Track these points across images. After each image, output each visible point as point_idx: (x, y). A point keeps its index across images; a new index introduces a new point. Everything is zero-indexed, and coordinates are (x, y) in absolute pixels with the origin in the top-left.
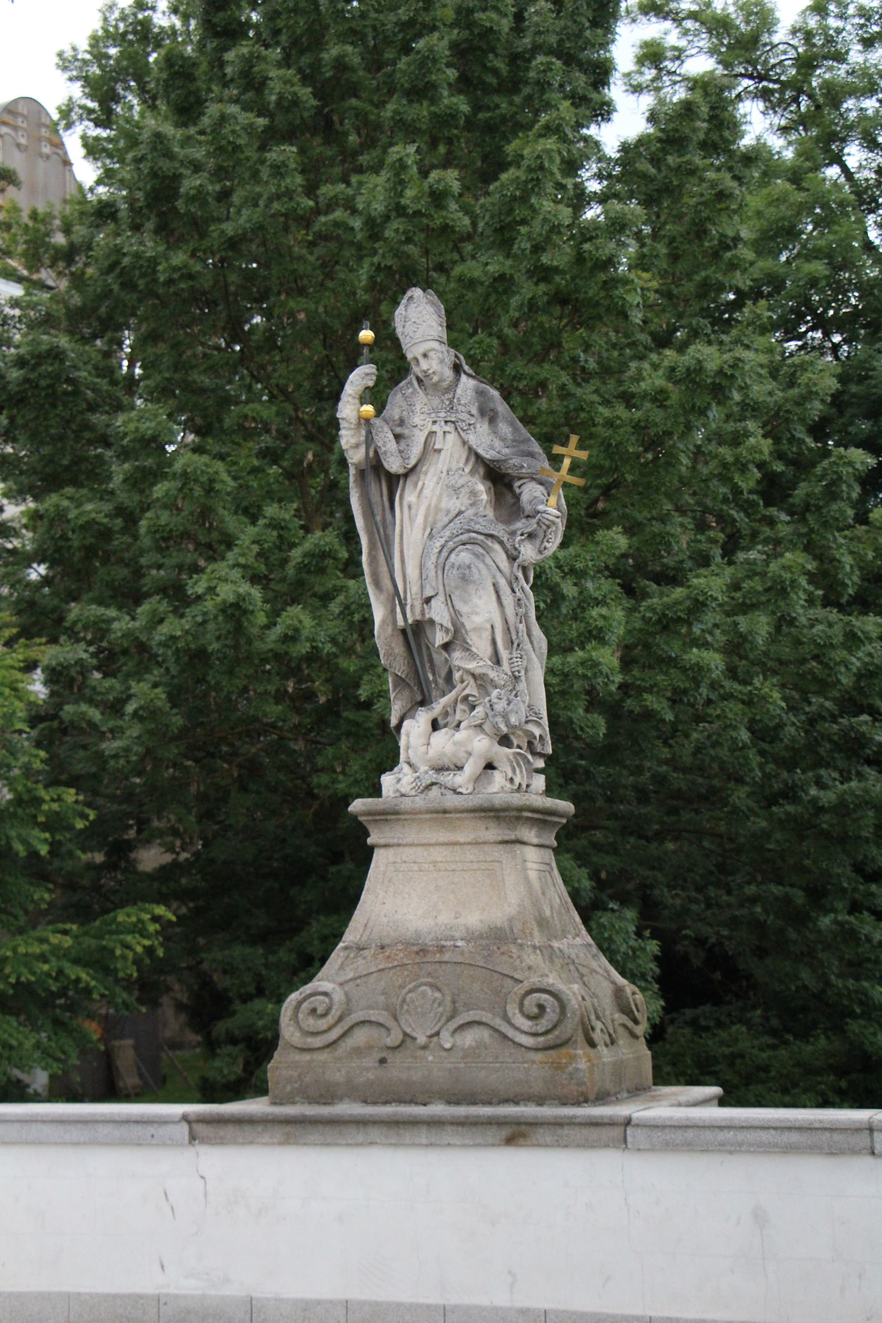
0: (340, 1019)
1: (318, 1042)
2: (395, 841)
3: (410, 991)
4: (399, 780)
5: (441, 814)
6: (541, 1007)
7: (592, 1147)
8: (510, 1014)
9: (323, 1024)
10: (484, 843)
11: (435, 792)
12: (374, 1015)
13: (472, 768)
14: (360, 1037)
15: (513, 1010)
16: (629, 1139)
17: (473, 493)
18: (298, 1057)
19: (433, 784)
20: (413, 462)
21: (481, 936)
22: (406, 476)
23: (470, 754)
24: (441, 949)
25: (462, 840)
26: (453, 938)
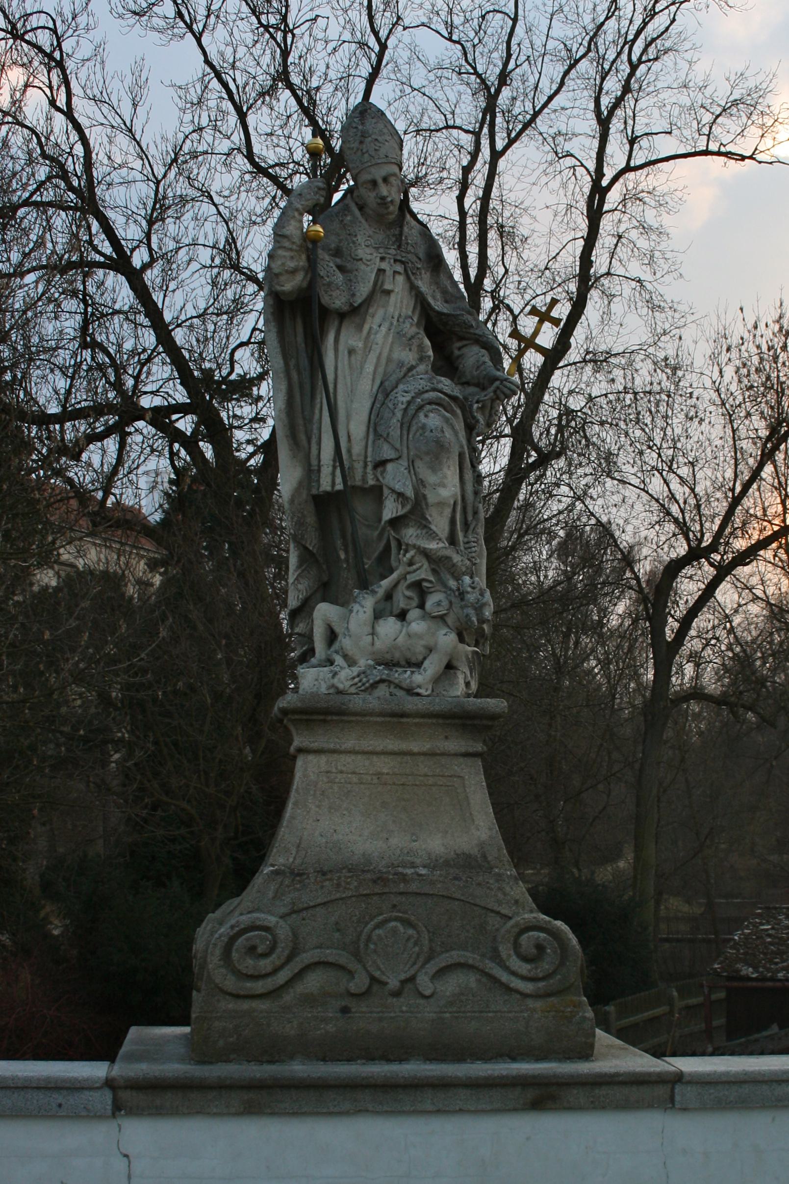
0: (289, 959)
1: (259, 987)
2: (332, 746)
3: (377, 926)
4: (335, 674)
5: (396, 719)
6: (540, 948)
7: (603, 1108)
8: (504, 955)
9: (265, 965)
10: (443, 754)
11: (382, 691)
12: (330, 955)
13: (432, 666)
14: (313, 982)
15: (506, 950)
16: (677, 1098)
17: (421, 347)
18: (232, 1005)
19: (382, 681)
20: (358, 300)
21: (447, 863)
22: (342, 316)
23: (430, 650)
24: (404, 878)
25: (416, 750)
26: (413, 865)
